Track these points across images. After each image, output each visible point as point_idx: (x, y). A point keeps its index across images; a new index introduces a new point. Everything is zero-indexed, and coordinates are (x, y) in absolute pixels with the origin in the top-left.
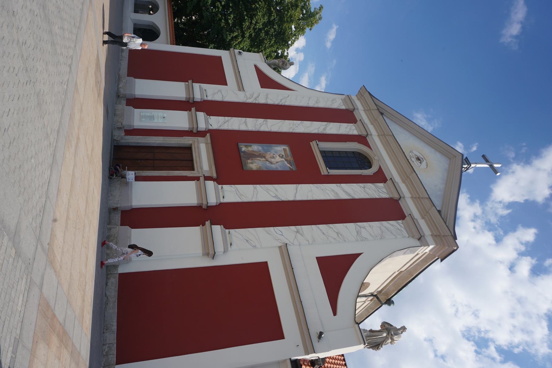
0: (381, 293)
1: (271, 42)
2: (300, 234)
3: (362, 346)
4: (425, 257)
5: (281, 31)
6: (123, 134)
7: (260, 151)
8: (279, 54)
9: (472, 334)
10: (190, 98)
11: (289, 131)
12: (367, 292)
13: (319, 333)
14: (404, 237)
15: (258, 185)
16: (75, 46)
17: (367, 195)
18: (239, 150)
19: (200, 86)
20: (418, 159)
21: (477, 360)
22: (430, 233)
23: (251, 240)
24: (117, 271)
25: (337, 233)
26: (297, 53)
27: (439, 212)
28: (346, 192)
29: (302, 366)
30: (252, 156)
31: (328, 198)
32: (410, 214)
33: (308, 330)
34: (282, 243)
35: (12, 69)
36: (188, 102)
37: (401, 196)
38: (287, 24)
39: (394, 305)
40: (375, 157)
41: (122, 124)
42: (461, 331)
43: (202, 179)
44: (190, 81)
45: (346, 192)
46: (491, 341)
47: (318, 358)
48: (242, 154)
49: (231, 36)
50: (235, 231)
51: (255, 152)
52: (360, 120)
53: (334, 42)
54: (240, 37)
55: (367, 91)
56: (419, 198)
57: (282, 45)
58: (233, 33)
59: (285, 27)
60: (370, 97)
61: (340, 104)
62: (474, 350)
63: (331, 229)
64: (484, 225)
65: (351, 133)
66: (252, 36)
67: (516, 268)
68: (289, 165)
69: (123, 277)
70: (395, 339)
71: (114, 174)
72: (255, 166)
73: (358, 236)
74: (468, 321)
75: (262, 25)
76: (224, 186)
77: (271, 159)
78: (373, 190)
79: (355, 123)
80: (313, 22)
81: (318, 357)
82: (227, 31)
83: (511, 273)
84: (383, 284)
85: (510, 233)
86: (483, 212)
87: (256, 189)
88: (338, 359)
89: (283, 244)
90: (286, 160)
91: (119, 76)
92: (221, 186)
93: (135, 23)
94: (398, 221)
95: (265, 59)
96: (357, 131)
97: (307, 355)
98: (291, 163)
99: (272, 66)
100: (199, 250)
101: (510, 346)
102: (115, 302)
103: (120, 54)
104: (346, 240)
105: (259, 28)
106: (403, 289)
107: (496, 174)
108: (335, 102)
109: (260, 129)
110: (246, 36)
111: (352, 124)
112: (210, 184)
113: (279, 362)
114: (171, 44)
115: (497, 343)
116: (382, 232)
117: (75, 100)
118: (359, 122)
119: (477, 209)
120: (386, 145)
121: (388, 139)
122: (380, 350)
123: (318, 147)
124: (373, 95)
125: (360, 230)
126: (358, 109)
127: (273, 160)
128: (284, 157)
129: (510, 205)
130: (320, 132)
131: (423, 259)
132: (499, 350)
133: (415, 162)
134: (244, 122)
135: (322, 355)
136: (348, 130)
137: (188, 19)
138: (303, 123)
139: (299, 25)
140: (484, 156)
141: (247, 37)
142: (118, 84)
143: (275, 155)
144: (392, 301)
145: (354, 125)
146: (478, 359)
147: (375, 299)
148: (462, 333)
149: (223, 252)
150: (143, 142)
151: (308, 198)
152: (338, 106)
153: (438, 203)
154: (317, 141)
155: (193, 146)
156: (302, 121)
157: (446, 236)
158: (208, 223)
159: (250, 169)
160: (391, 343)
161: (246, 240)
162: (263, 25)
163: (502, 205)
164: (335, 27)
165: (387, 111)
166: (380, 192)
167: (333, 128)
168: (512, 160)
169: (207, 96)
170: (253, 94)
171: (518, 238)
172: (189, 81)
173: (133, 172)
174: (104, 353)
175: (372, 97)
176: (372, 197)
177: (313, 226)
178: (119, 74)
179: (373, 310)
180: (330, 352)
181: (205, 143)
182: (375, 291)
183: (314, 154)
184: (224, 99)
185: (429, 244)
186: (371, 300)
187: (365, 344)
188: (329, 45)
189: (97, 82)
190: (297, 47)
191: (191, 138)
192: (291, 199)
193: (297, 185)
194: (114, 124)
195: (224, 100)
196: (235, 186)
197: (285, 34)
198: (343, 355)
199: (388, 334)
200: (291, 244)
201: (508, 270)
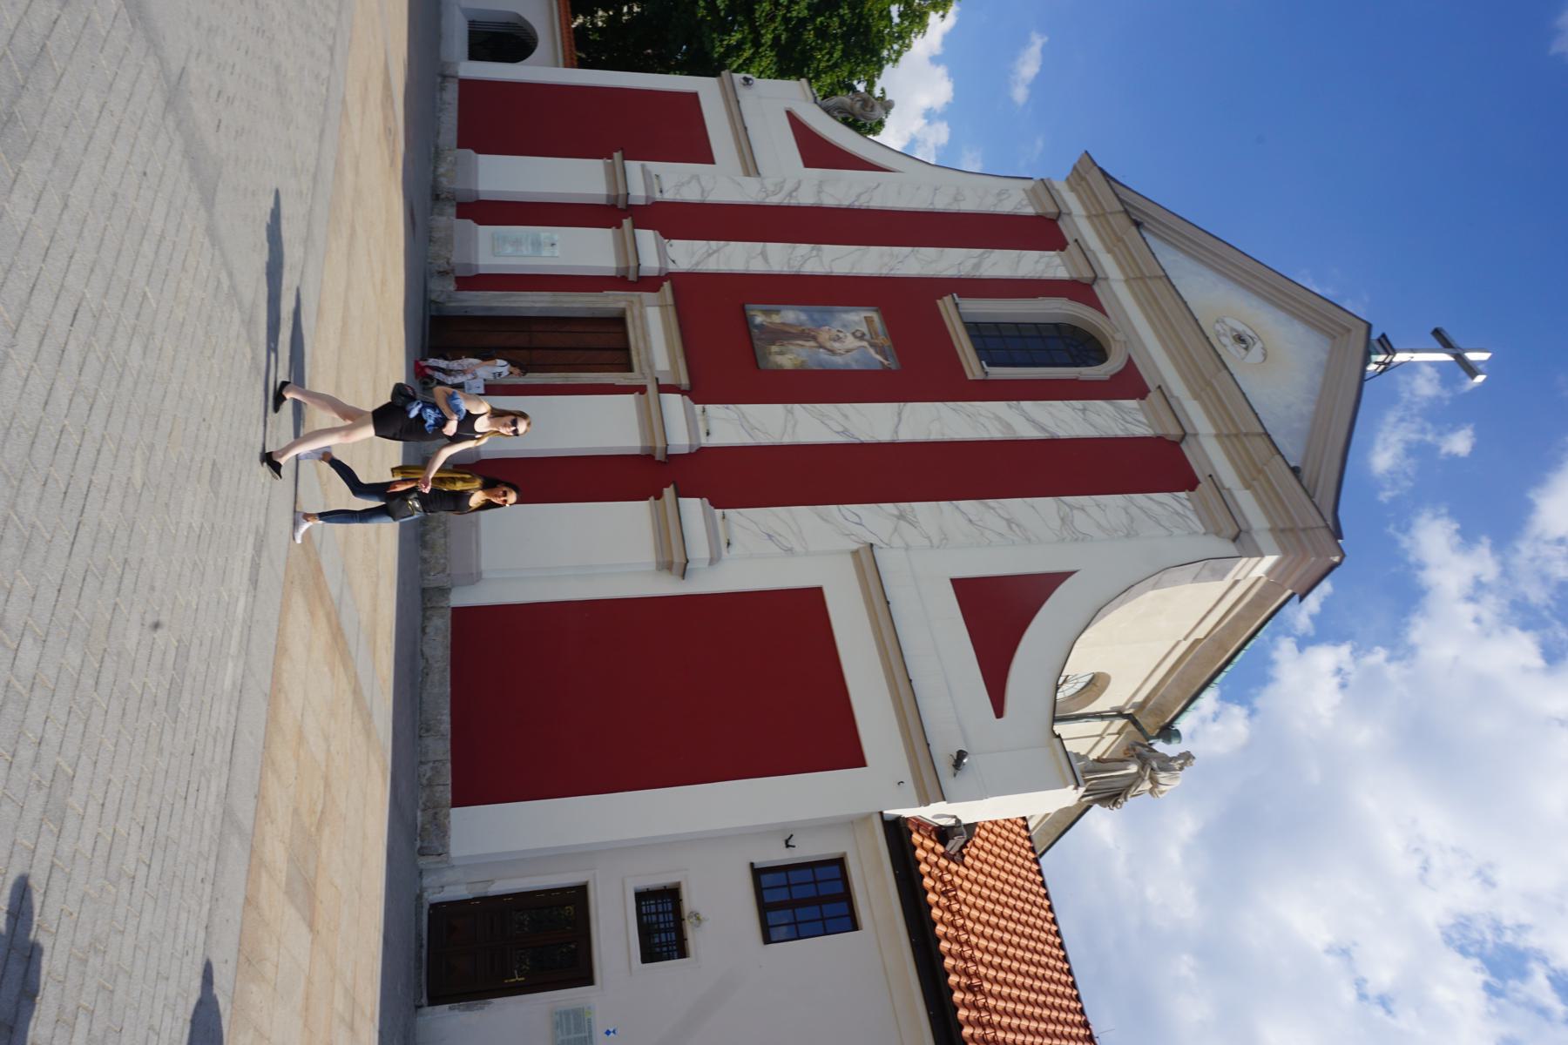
0: (1146, 710)
1: (832, 56)
4: (1258, 595)
6: (452, 287)
7: (801, 325)
9: (1476, 936)
10: (628, 268)
11: (879, 272)
12: (1102, 704)
13: (955, 755)
17: (1092, 428)
18: (746, 321)
19: (643, 166)
20: (1240, 339)
23: (780, 535)
25: (1007, 520)
26: (930, 123)
27: (1295, 471)
28: (1033, 421)
29: (911, 833)
30: (783, 335)
34: (858, 543)
39: (1179, 742)
41: (448, 263)
44: (617, 156)
46: (1537, 959)
47: (952, 822)
49: (725, 43)
52: (1076, 241)
53: (1039, 84)
55: (1095, 164)
56: (1236, 436)
57: (864, 61)
59: (870, 10)
61: (1020, 202)
63: (992, 511)
65: (1050, 274)
66: (781, 40)
68: (879, 357)
69: (461, 614)
70: (1162, 781)
72: (791, 359)
74: (1464, 896)
75: (806, 8)
76: (709, 407)
77: (832, 342)
78: (1107, 415)
81: (955, 817)
86: (1506, 572)
87: (792, 413)
90: (872, 345)
92: (721, 510)
93: (471, 19)
94: (1176, 493)
95: (814, 94)
99: (836, 113)
105: (797, 17)
110: (763, 41)
112: (673, 403)
113: (852, 822)
114: (566, 66)
115: (1556, 964)
116: (1132, 520)
118: (1072, 247)
119: (1483, 563)
120: (1149, 304)
121: (1113, 222)
122: (1121, 807)
126: (1070, 214)
127: (836, 345)
128: (866, 337)
133: (1230, 348)
136: (1040, 267)
137: (609, 16)
140: (1437, 333)
141: (766, 46)
142: (436, 168)
143: (841, 332)
144: (1177, 730)
146: (1493, 1009)
147: (1131, 728)
148: (1443, 933)
149: (708, 561)
150: (501, 305)
154: (955, 295)
155: (629, 314)
157: (1312, 528)
158: (669, 492)
159: (775, 368)
160: (1151, 791)
164: (1038, 42)
165: (1153, 218)
169: (661, 192)
174: (424, 781)
175: (1112, 183)
176: (1104, 435)
177: (944, 505)
180: (985, 800)
181: (660, 306)
182: (1126, 704)
185: (1264, 551)
186: (1119, 733)
187: (1078, 786)
188: (1020, 94)
189: (388, 131)
190: (929, 107)
193: (902, 404)
198: (1024, 819)
199: (1143, 767)
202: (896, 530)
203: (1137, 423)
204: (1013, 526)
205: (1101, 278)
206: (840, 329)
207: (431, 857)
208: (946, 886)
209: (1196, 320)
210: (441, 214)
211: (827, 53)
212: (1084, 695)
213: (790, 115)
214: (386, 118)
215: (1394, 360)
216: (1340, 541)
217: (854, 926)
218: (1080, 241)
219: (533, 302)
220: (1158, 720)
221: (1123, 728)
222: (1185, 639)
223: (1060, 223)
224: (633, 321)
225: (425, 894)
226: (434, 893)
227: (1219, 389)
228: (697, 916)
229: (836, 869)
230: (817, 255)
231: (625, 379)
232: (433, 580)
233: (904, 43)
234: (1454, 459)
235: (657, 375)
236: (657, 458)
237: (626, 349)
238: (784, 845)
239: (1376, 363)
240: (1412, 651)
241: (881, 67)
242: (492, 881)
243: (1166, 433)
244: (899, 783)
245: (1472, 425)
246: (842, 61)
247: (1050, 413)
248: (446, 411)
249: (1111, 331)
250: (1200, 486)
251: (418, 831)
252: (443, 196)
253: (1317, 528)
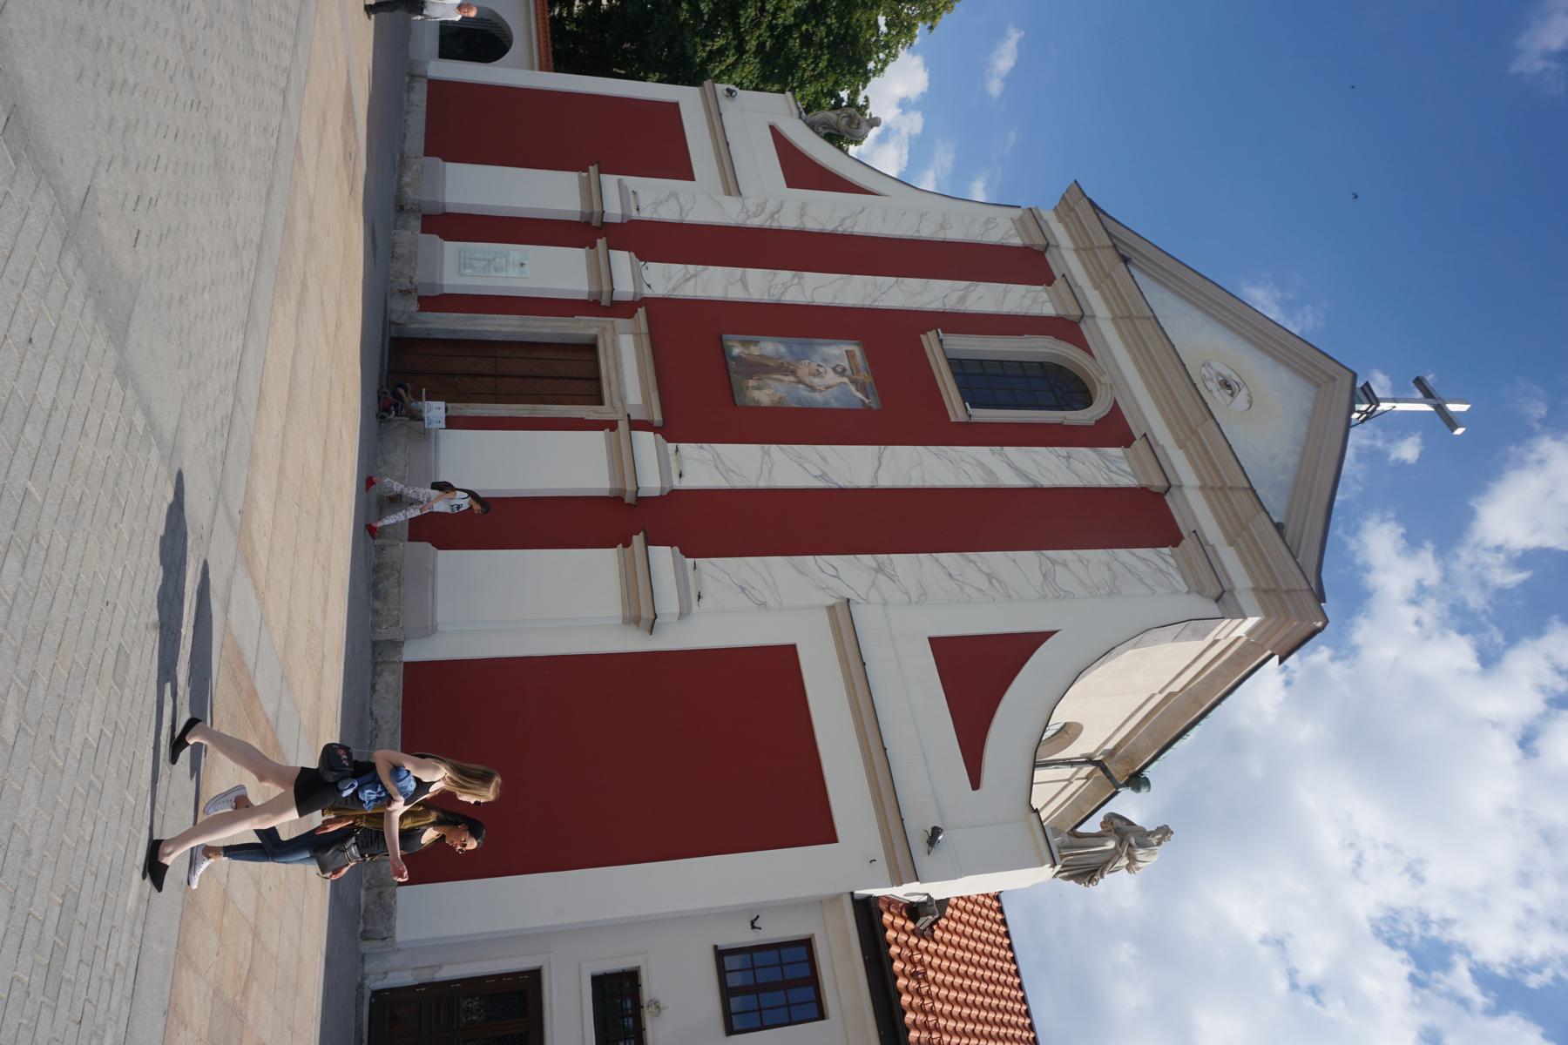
0: (1116, 757)
1: (817, 65)
2: (885, 575)
3: (1047, 872)
4: (1236, 653)
5: (846, 33)
6: (414, 307)
7: (781, 358)
8: (843, 101)
9: (1403, 928)
10: (592, 214)
11: (862, 303)
12: (1074, 751)
14: (1176, 591)
15: (774, 447)
16: (295, 46)
17: (1074, 476)
18: (723, 353)
19: (619, 182)
20: (1226, 384)
21: (1414, 1004)
22: (1249, 584)
23: (753, 588)
24: (400, 656)
26: (904, 113)
27: (1279, 527)
28: (1017, 469)
29: (882, 913)
30: (761, 368)
31: (965, 483)
32: (1195, 531)
33: (882, 752)
35: (162, 64)
36: (588, 224)
37: (1172, 483)
38: (862, 13)
39: (1149, 791)
40: (1101, 378)
41: (410, 282)
42: (1370, 919)
43: (623, 426)
44: (593, 169)
46: (1461, 952)
49: (708, 49)
51: (769, 358)
52: (1064, 275)
53: (1010, 79)
54: (733, 51)
55: (1084, 195)
56: (1221, 489)
57: (849, 72)
58: (713, 41)
59: (858, 20)
60: (1092, 212)
61: (1007, 233)
62: (1405, 975)
63: (972, 565)
64: (1447, 614)
65: (1036, 311)
67: (1539, 744)
68: (859, 395)
69: (415, 671)
70: (1139, 858)
71: (392, 408)
72: (768, 395)
73: (1047, 585)
75: (792, 16)
76: (681, 446)
78: (1092, 464)
79: (1050, 284)
80: (937, 7)
81: (927, 894)
82: (697, 34)
83: (1525, 758)
84: (1118, 729)
85: (1526, 641)
86: (1446, 578)
87: (769, 455)
88: (983, 905)
89: (839, 601)
90: (853, 382)
91: (402, 156)
92: (693, 560)
95: (799, 108)
96: (1054, 307)
97: (897, 886)
98: (865, 389)
99: (820, 129)
100: (613, 608)
101: (1514, 966)
102: (395, 732)
103: (406, 98)
105: (783, 24)
106: (1175, 746)
107: (1453, 431)
108: (993, 228)
109: (783, 299)
110: (747, 48)
111: (1039, 288)
113: (821, 902)
114: (541, 69)
115: (1477, 957)
117: (296, 184)
118: (1059, 282)
119: (1425, 567)
120: (1137, 345)
123: (943, 349)
124: (1101, 207)
125: (1052, 570)
126: (1057, 246)
129: (1527, 559)
130: (948, 307)
131: (1230, 658)
132: (1483, 977)
133: (1216, 394)
135: (939, 890)
137: (587, 6)
138: (902, 282)
139: (898, 16)
140: (1419, 382)
141: (751, 52)
142: (400, 177)
143: (821, 366)
144: (1146, 779)
145: (1047, 291)
146: (1417, 1000)
147: (1100, 773)
148: (1372, 926)
149: (677, 615)
150: (466, 328)
151: (910, 481)
152: (1003, 238)
153: (1277, 506)
154: (939, 330)
156: (900, 279)
157: (1295, 591)
158: (638, 540)
159: (752, 404)
161: (741, 587)
162: (795, 15)
163: (1502, 556)
164: (1014, 37)
166: (1111, 472)
167: (985, 297)
168: (1537, 426)
169: (638, 209)
171: (1548, 657)
172: (591, 168)
173: (442, 404)
175: (1101, 215)
177: (924, 557)
178: (403, 151)
179: (1092, 805)
181: (633, 334)
182: (1097, 751)
183: (925, 352)
184: (686, 216)
186: (1087, 778)
187: (1054, 865)
188: (995, 87)
189: (348, 156)
191: (597, 321)
192: (864, 482)
193: (883, 447)
194: (391, 282)
195: (686, 219)
196: (713, 448)
197: (858, 41)
198: (997, 898)
199: (1120, 844)
200: (860, 601)
201: (1516, 747)
202: (873, 583)
203: (1122, 473)
204: (995, 582)
205: (1052, 246)
207: (374, 942)
208: (916, 967)
209: (1184, 365)
210: (405, 227)
211: (812, 63)
212: (1055, 742)
213: (774, 130)
214: (345, 144)
215: (1379, 409)
216: (1323, 604)
217: (821, 1015)
218: (1067, 276)
219: (500, 325)
220: (1128, 767)
221: (1091, 773)
222: (1160, 692)
223: (1047, 255)
224: (605, 349)
225: (367, 982)
226: (376, 980)
227: (1261, 544)
228: (656, 1004)
229: (802, 950)
230: (798, 284)
231: (595, 412)
232: (385, 633)
233: (890, 52)
234: (1401, 465)
235: (628, 411)
236: (627, 501)
237: (597, 379)
238: (750, 927)
239: (1359, 412)
240: (1355, 651)
241: (867, 80)
242: (440, 966)
243: (1150, 484)
244: (871, 862)
245: (1420, 433)
246: (828, 72)
247: (1034, 460)
248: (392, 788)
249: (1097, 374)
250: (1184, 542)
251: (362, 912)
252: (408, 207)
253: (1301, 590)
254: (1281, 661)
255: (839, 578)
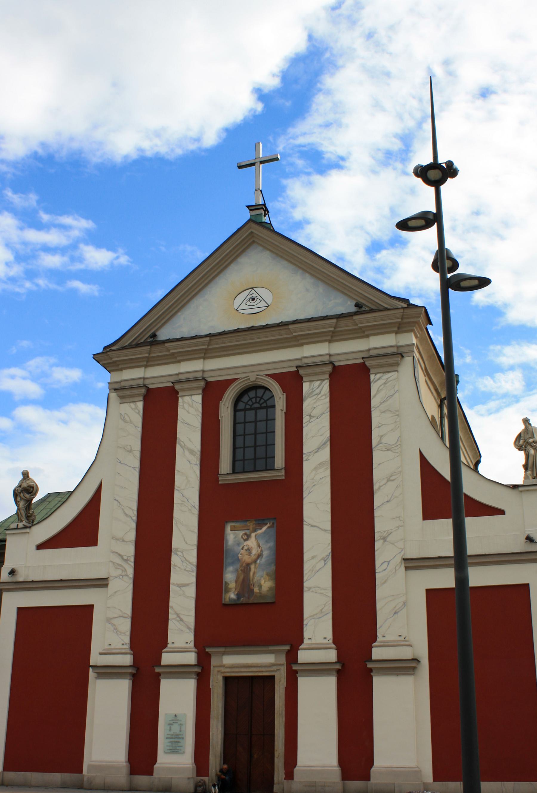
2: (388, 536)
7: (237, 570)
15: (305, 584)
25: (387, 481)
28: (319, 448)
40: (252, 380)
45: (319, 448)
48: (242, 600)
50: (380, 627)
63: (381, 488)
68: (264, 529)
72: (265, 582)
87: (310, 588)
90: (255, 531)
104: (400, 470)
134: (179, 589)
157: (403, 315)
170: (113, 562)
192: (328, 537)
193: (304, 523)
200: (403, 553)
206: (241, 547)
213: (40, 547)
230: (182, 552)
254: (431, 324)
255: (390, 561)
